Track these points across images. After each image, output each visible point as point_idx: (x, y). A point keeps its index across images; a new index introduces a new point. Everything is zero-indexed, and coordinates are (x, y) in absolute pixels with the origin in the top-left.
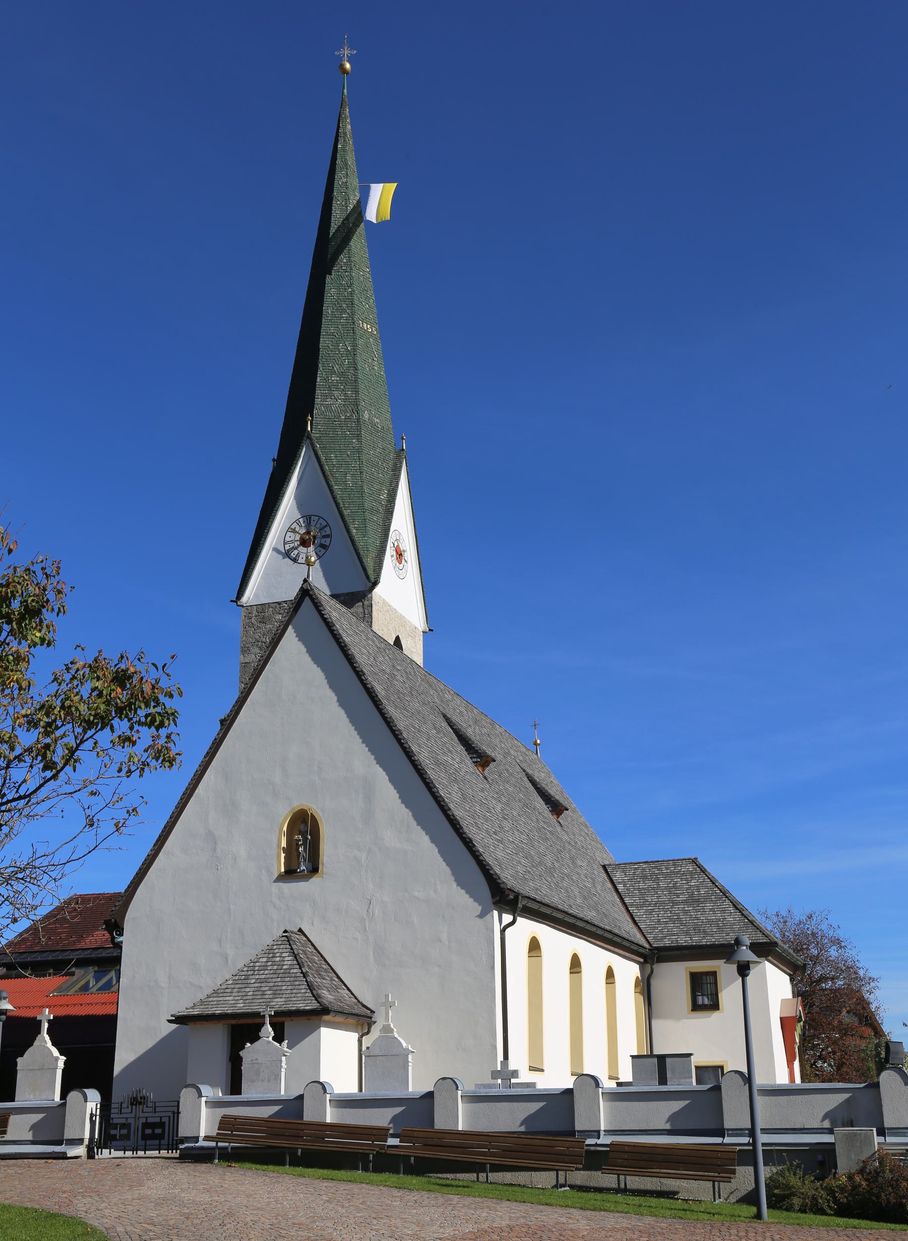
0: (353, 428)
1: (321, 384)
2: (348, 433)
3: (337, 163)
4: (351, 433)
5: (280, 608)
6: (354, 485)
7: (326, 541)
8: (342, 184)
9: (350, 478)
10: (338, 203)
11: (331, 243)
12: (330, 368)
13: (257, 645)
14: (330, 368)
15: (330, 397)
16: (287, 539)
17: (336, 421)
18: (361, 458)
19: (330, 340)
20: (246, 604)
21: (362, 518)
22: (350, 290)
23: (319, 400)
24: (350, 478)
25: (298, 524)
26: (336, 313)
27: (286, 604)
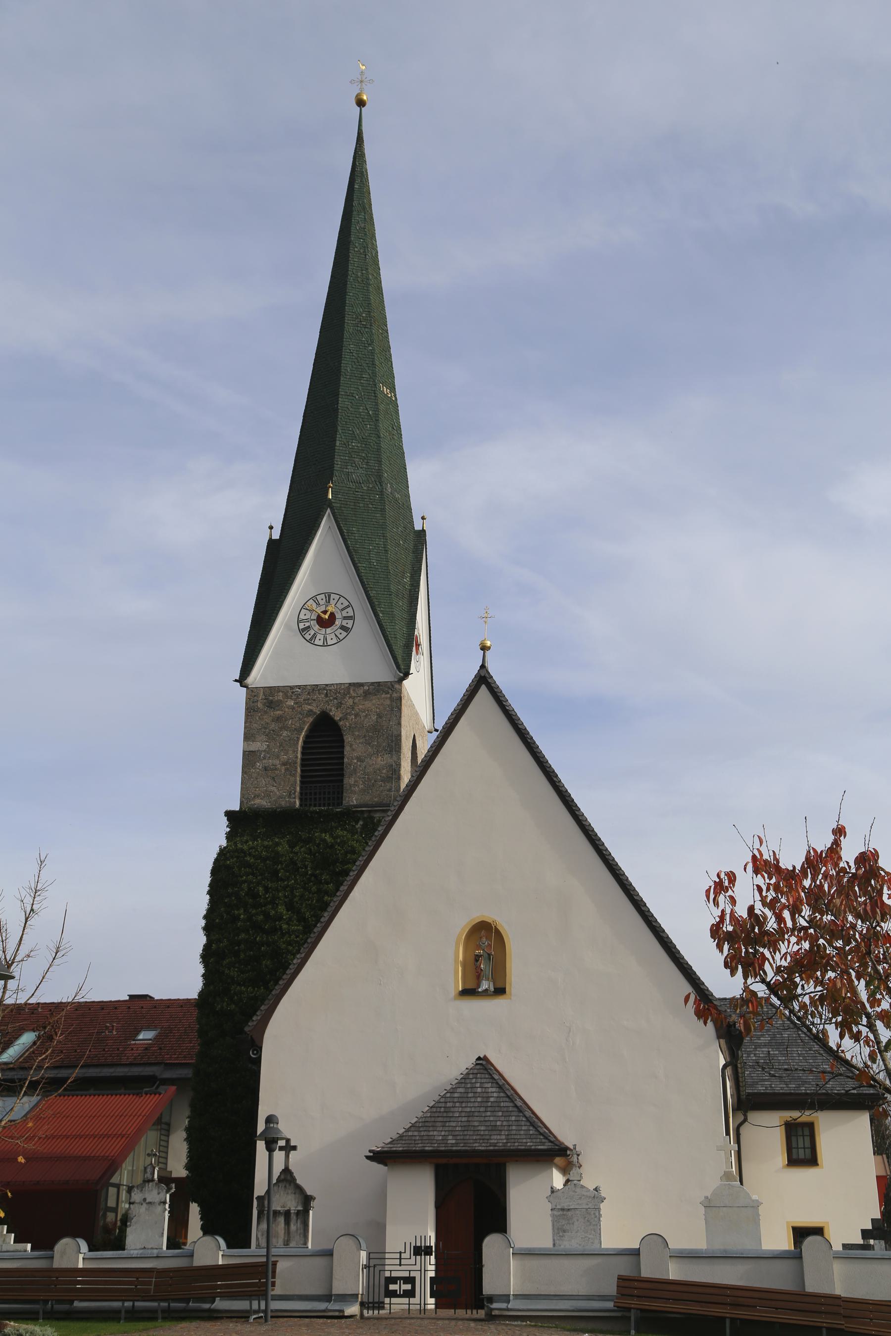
0: (376, 501)
1: (341, 448)
2: (371, 506)
3: (354, 205)
4: (374, 506)
5: (293, 693)
6: (379, 564)
7: (349, 624)
8: (359, 229)
9: (374, 556)
10: (356, 249)
11: (349, 294)
12: (350, 432)
13: (264, 732)
14: (350, 432)
15: (350, 464)
16: (302, 617)
17: (357, 492)
18: (385, 535)
19: (351, 401)
20: (251, 685)
21: (388, 601)
22: (371, 348)
23: (339, 466)
24: (374, 556)
25: (315, 601)
26: (355, 372)
27: (299, 689)
